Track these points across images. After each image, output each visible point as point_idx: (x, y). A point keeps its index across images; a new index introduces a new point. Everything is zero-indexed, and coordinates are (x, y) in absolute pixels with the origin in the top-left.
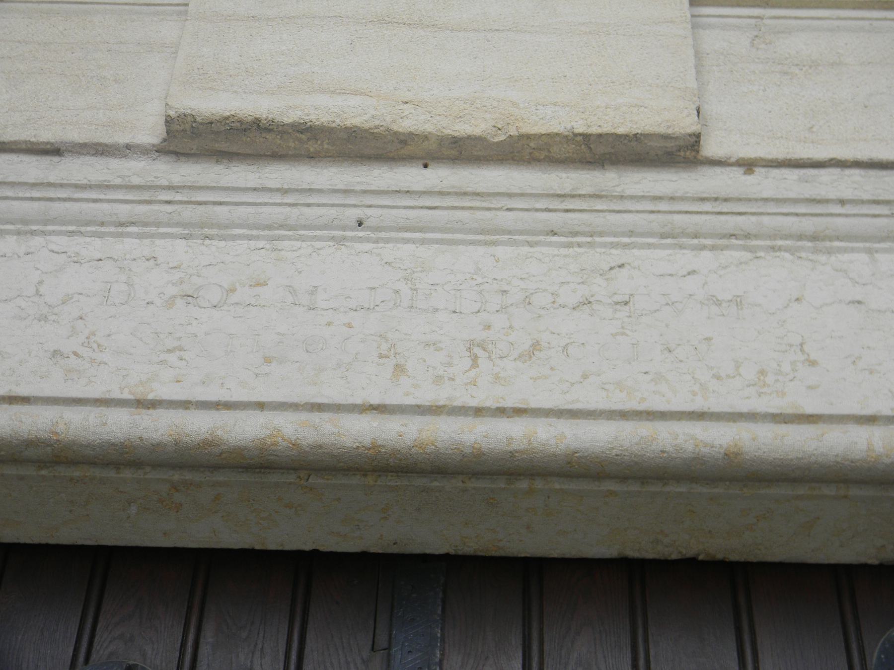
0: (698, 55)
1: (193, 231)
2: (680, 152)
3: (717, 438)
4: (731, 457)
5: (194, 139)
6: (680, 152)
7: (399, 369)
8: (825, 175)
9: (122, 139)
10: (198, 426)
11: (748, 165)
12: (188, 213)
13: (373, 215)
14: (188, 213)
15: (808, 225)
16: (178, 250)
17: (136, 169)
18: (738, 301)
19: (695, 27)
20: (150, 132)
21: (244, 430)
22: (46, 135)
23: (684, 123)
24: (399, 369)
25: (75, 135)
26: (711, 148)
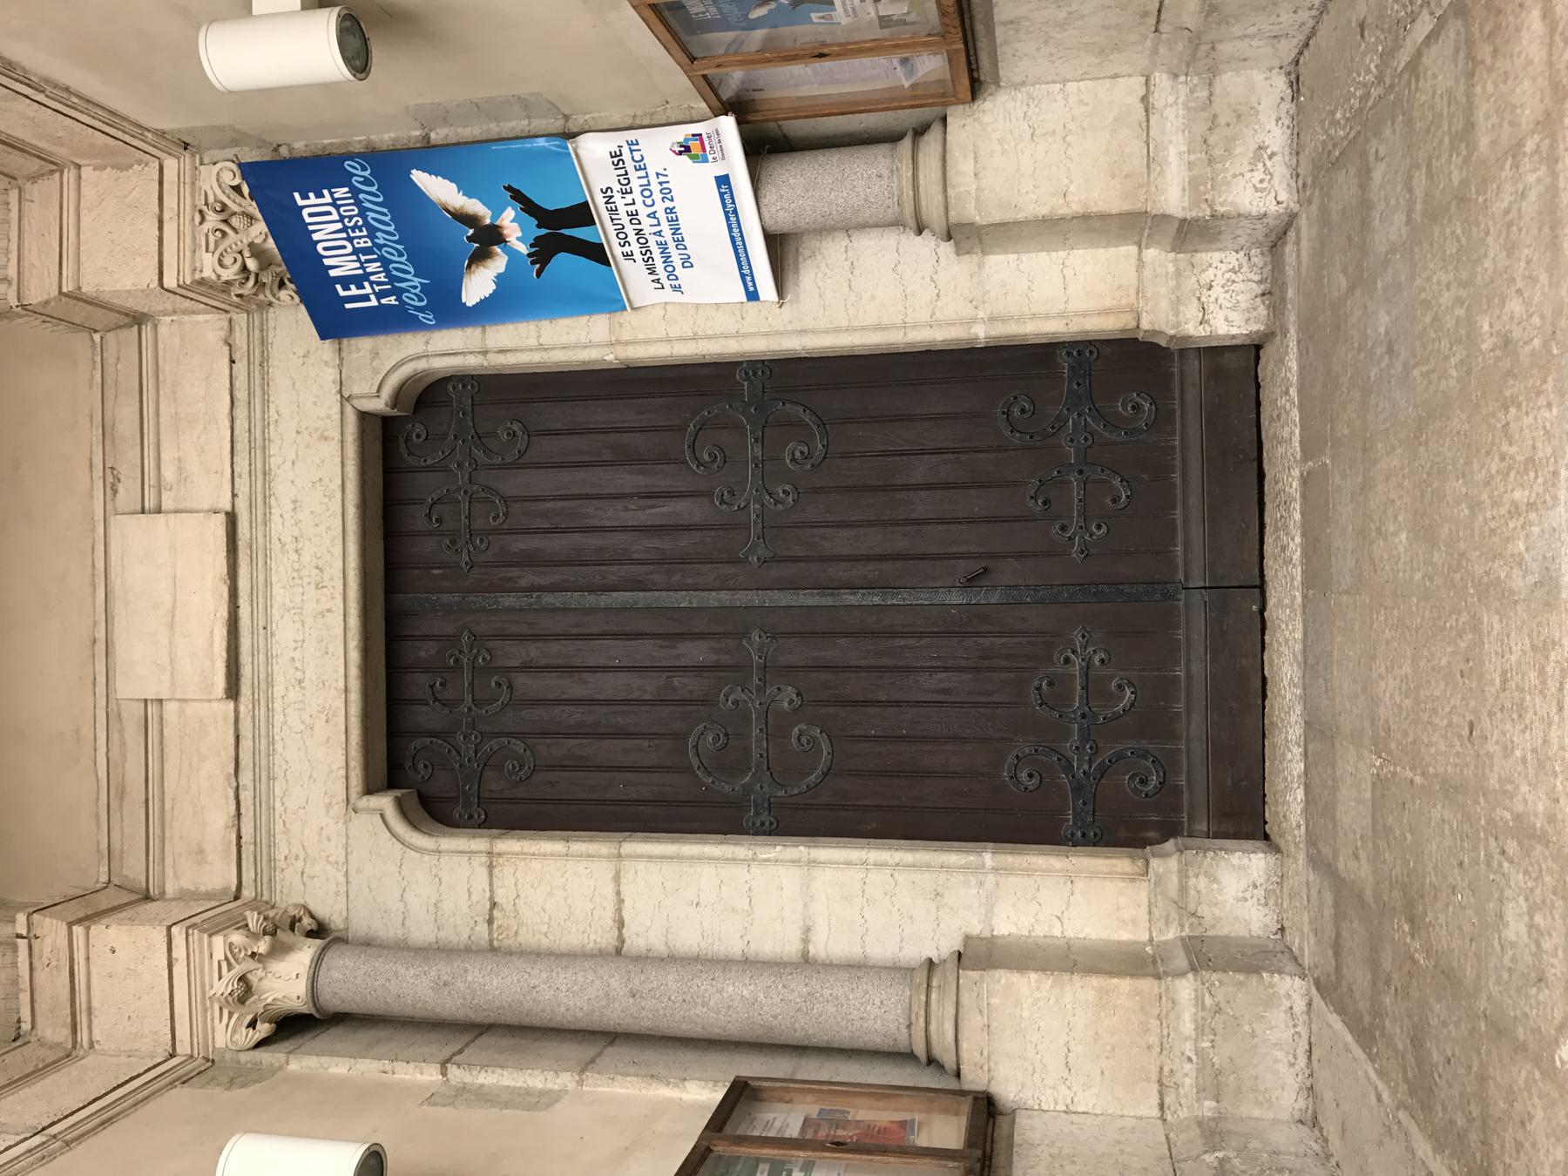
0: (176, 512)
1: (270, 683)
2: (232, 519)
3: (352, 511)
4: (358, 507)
5: (233, 690)
6: (232, 519)
7: (329, 611)
8: (237, 470)
9: (232, 714)
10: (354, 671)
11: (234, 495)
12: (263, 686)
13: (261, 624)
14: (263, 686)
15: (260, 477)
16: (278, 690)
17: (242, 708)
18: (294, 502)
19: (159, 512)
20: (231, 705)
21: (355, 656)
22: (232, 741)
23: (222, 517)
24: (329, 611)
25: (231, 731)
26: (228, 508)
